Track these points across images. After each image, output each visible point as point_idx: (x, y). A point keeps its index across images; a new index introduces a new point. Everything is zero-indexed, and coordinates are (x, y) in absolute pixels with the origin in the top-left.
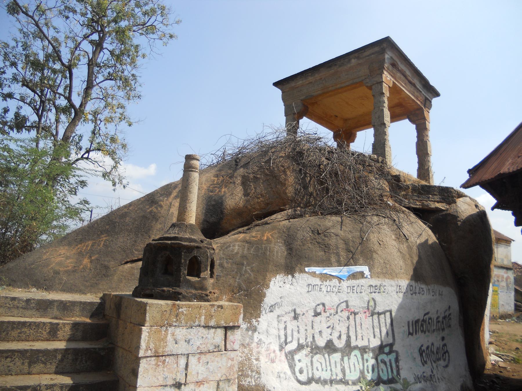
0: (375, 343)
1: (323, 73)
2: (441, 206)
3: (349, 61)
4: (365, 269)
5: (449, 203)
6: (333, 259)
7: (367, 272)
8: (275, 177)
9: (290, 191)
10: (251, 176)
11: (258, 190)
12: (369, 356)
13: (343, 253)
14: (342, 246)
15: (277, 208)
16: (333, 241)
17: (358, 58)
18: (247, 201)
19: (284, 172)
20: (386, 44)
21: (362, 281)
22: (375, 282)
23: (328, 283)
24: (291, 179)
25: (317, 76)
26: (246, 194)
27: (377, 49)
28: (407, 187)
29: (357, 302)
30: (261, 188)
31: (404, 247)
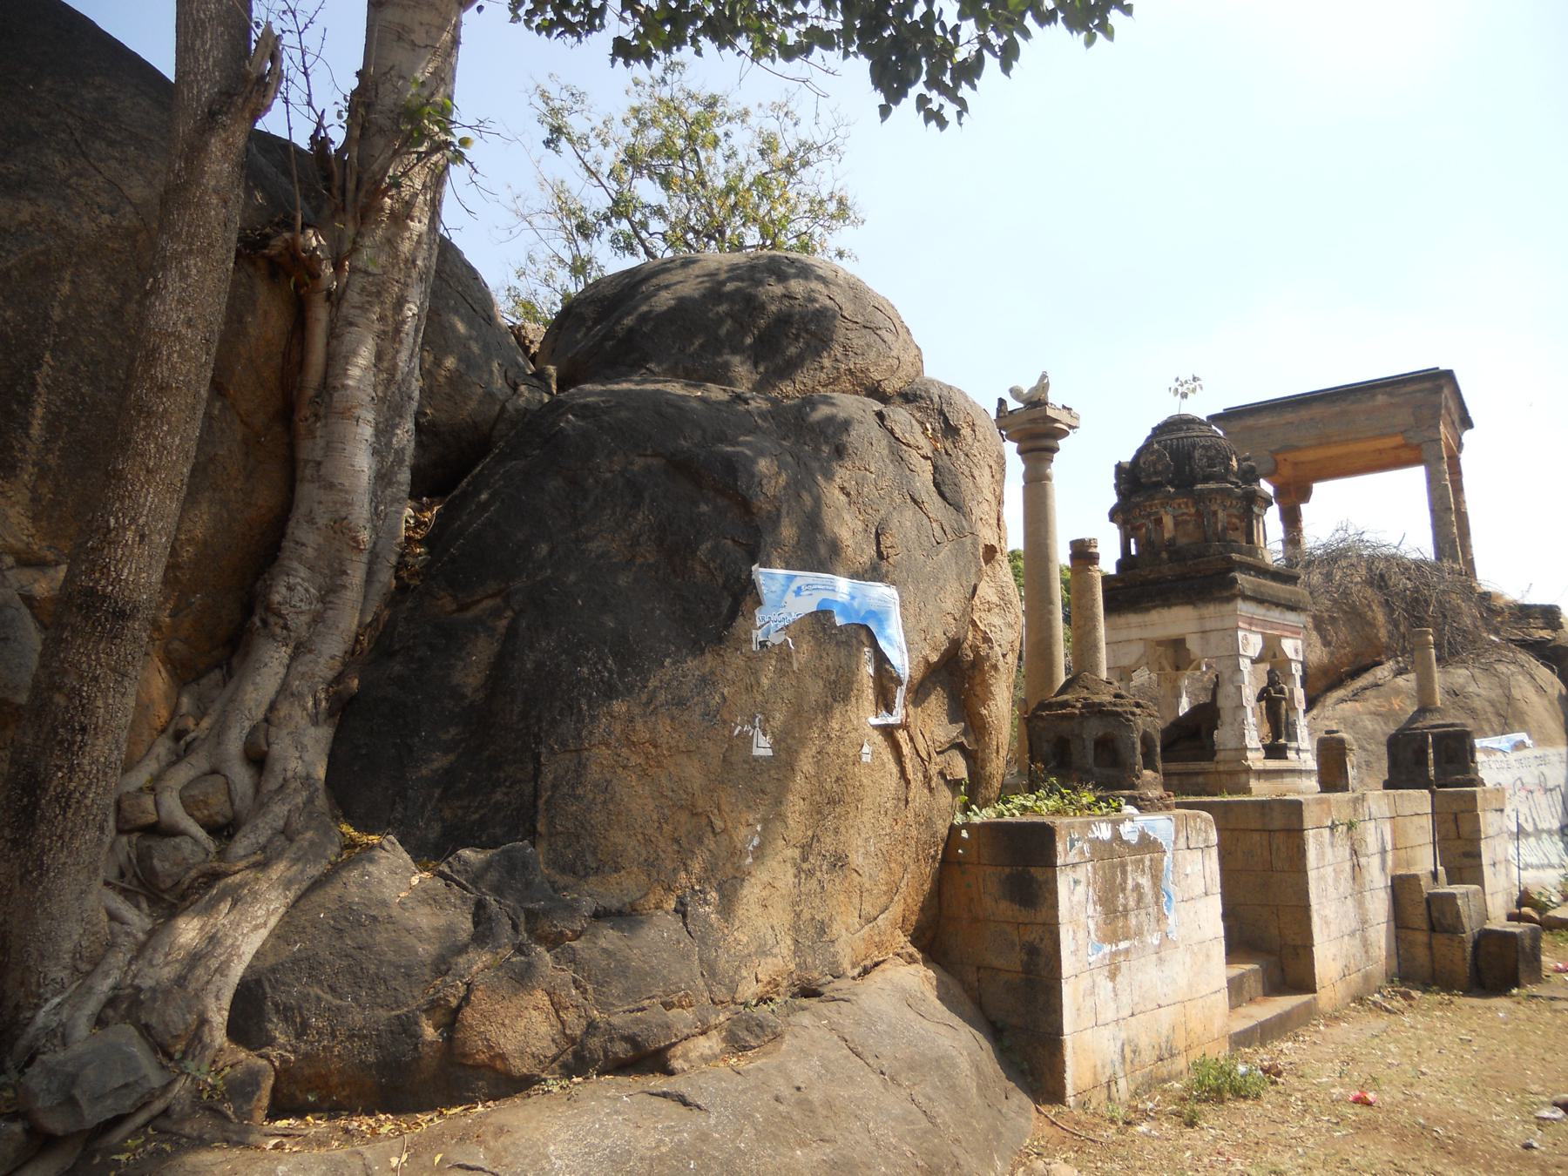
0: (1556, 825)
1: (1318, 410)
2: (1546, 634)
3: (1374, 396)
4: (1523, 736)
5: (1555, 630)
6: (1486, 728)
7: (1529, 742)
8: (1359, 615)
9: (1383, 634)
10: (1326, 615)
11: (1341, 636)
12: (1556, 838)
13: (1494, 719)
14: (1490, 709)
15: (1370, 661)
16: (1477, 703)
17: (1390, 395)
18: (1332, 654)
19: (1370, 606)
20: (1449, 376)
21: (1525, 753)
22: (1538, 752)
23: (1493, 758)
24: (1380, 617)
25: (1304, 413)
26: (1326, 643)
27: (1427, 385)
28: (1500, 612)
29: (1530, 780)
30: (1342, 633)
31: (1546, 702)
